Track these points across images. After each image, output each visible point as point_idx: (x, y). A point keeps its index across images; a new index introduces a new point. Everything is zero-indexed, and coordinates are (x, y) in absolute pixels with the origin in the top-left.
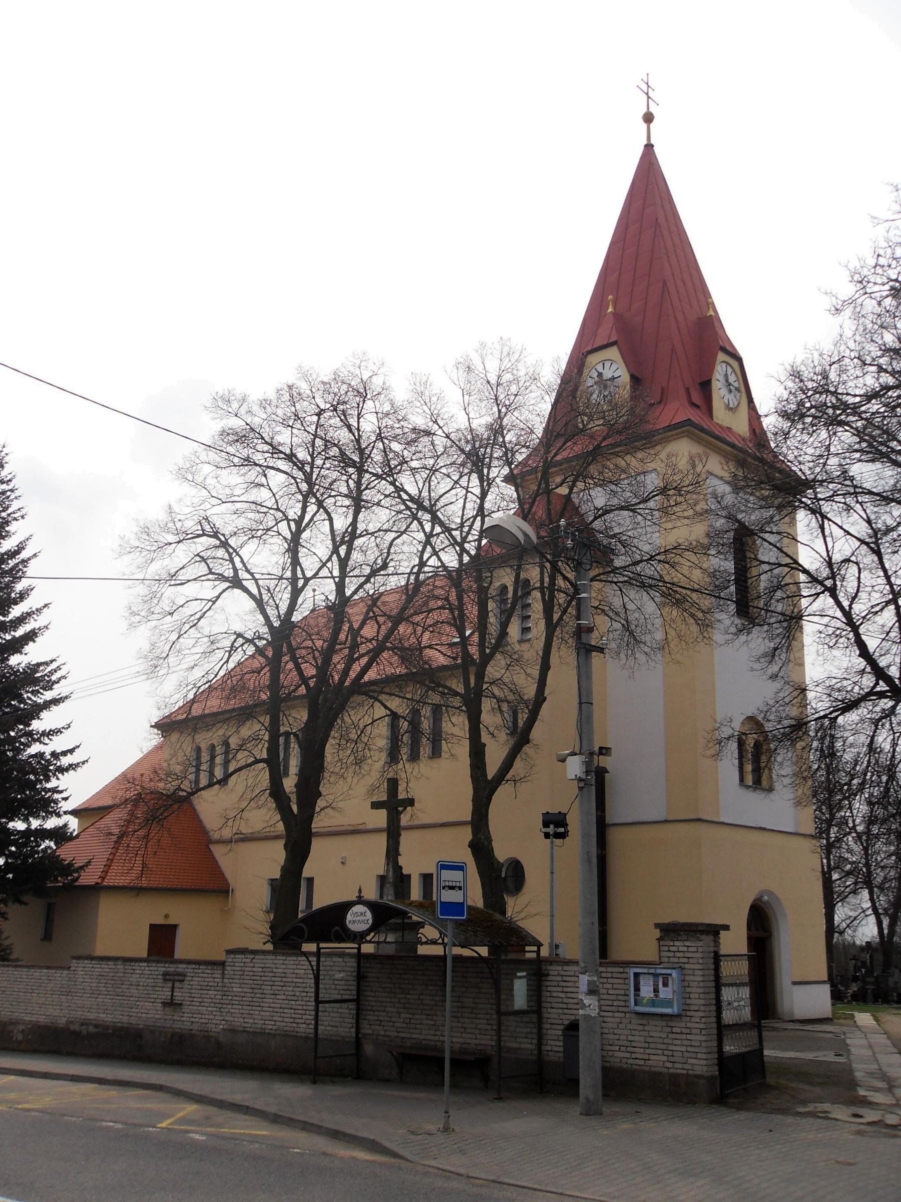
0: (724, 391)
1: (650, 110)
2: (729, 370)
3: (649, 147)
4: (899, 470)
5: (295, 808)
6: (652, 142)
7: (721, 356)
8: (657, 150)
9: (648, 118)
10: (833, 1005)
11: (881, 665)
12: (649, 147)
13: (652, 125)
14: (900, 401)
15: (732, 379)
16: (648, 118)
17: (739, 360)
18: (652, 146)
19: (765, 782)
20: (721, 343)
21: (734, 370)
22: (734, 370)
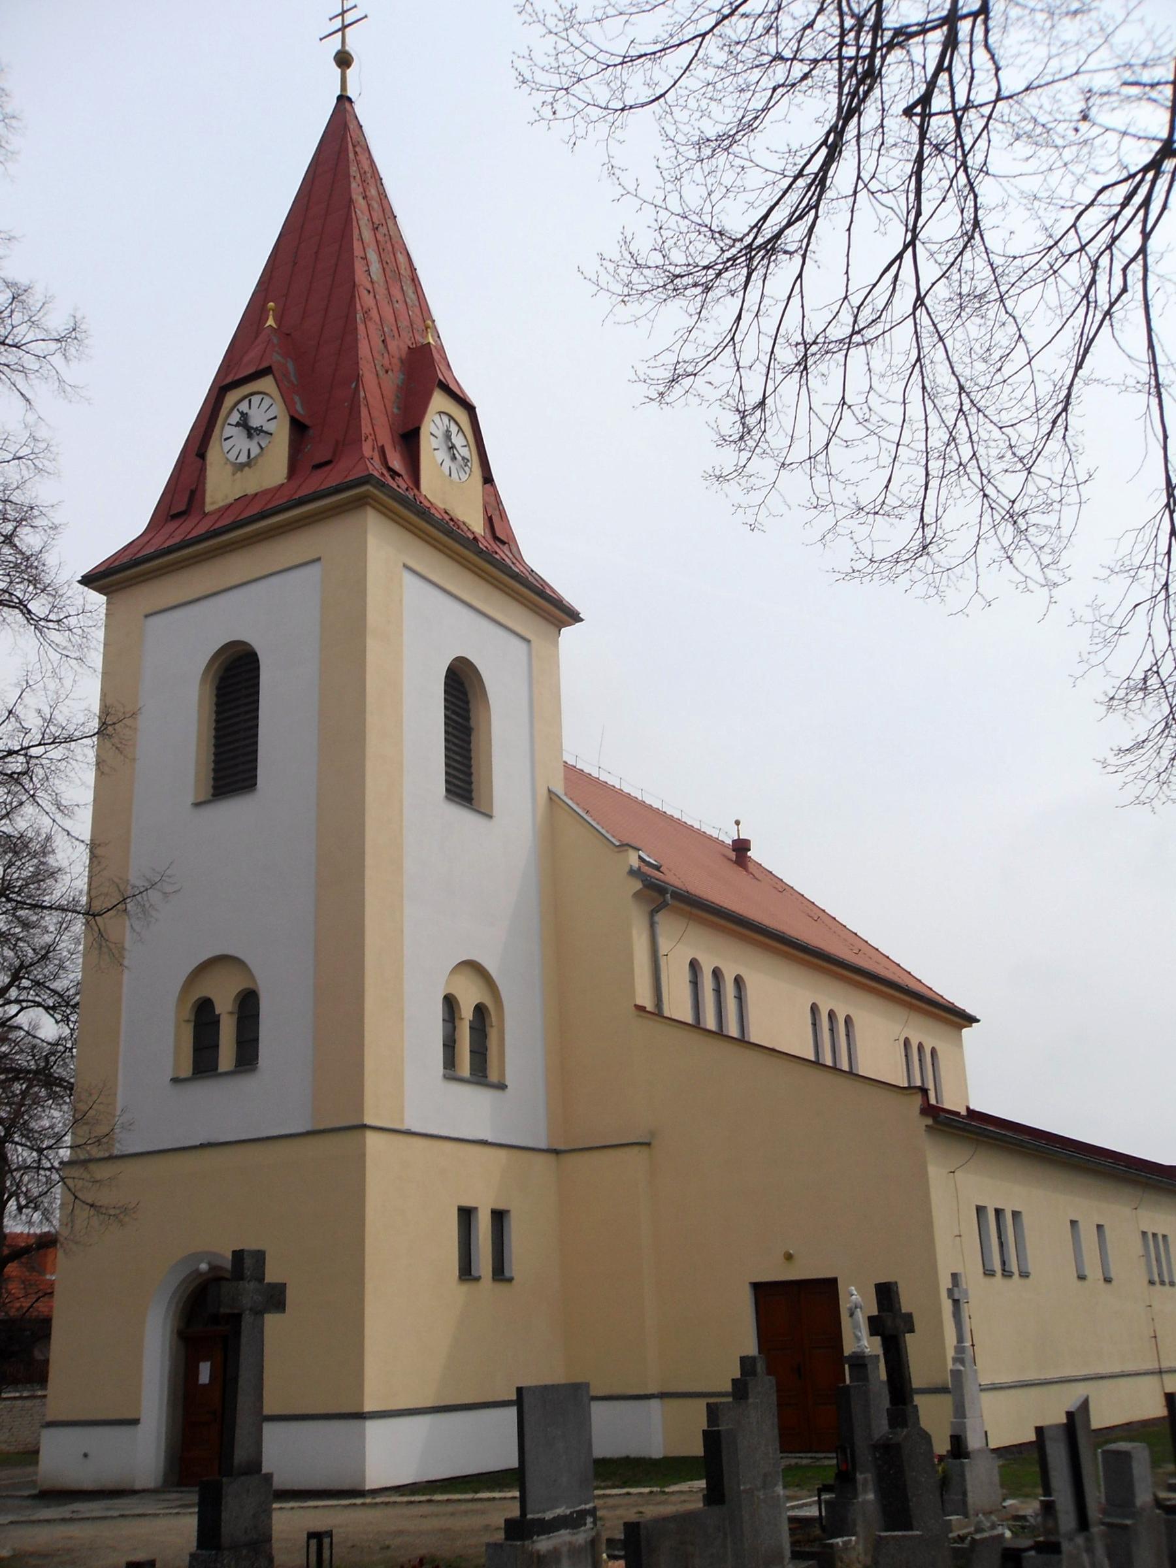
0: (442, 455)
1: (347, 48)
2: (454, 429)
3: (344, 100)
4: (5, 827)
5: (847, 1366)
6: (350, 93)
7: (439, 401)
8: (361, 110)
9: (343, 60)
10: (39, 1442)
11: (1165, 116)
12: (344, 100)
13: (349, 71)
14: (2, 1077)
15: (458, 440)
16: (343, 60)
17: (470, 409)
18: (350, 100)
19: (493, 1077)
20: (441, 377)
21: (460, 429)
22: (460, 429)
